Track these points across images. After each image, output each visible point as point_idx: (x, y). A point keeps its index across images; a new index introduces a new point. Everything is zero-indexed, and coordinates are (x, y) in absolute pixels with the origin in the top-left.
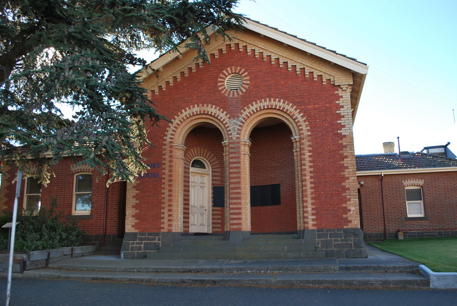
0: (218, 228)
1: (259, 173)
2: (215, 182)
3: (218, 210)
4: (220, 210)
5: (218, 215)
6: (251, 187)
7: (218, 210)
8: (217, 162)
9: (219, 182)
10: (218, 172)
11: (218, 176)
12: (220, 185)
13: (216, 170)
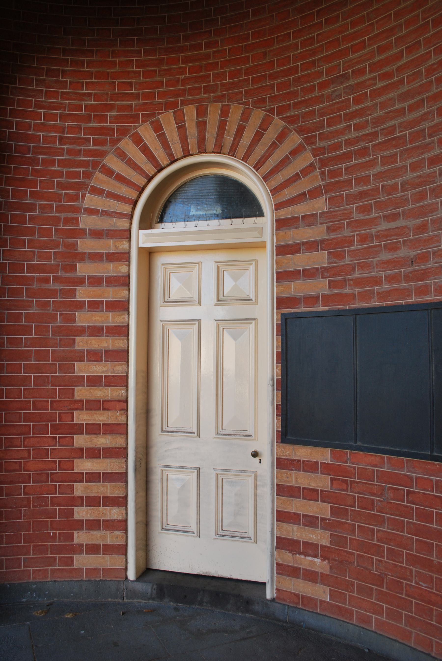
0: (311, 576)
1: (394, 217)
2: (298, 288)
3: (311, 467)
4: (327, 468)
5: (311, 494)
6: (292, 328)
7: (311, 467)
8: (307, 158)
9: (320, 286)
10: (310, 220)
11: (311, 246)
12: (326, 299)
13: (300, 209)
